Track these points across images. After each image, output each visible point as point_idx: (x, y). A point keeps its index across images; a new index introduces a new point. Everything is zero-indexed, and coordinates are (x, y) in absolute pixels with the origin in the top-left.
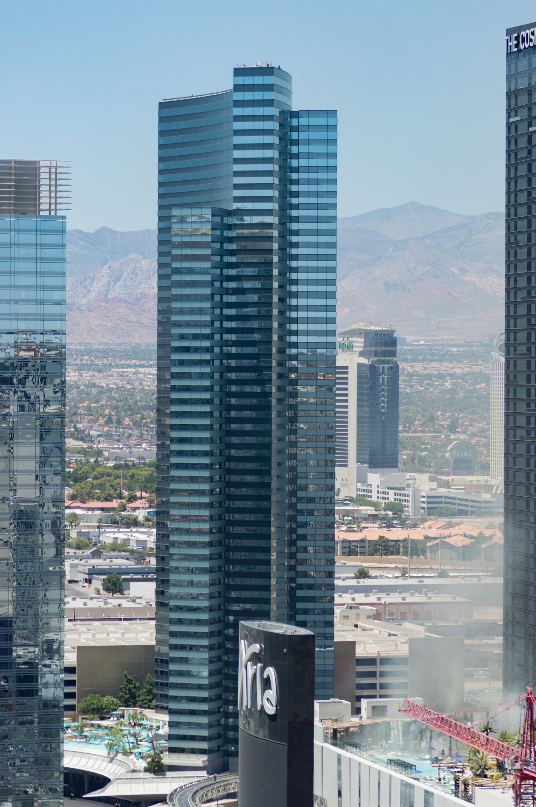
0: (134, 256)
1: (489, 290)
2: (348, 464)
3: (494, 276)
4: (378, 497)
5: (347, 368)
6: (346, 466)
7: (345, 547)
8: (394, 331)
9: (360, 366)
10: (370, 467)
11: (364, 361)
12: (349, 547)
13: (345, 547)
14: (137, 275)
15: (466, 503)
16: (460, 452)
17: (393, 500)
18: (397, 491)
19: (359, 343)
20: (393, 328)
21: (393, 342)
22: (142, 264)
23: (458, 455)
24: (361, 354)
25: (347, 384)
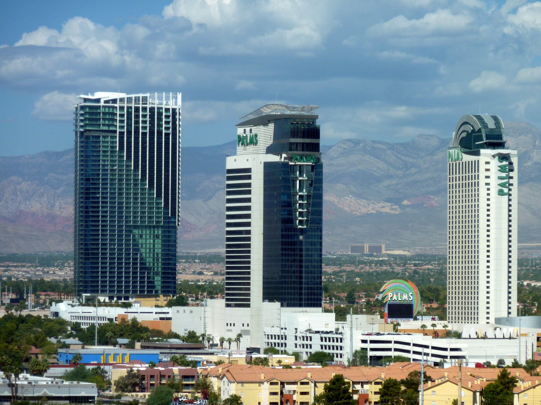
0: (14, 178)
1: (346, 209)
2: (251, 303)
3: (351, 196)
4: (296, 345)
5: (249, 170)
6: (248, 306)
7: (275, 394)
8: (316, 117)
9: (268, 166)
10: (282, 306)
11: (274, 158)
12: (282, 393)
13: (275, 394)
14: (17, 195)
15: (426, 350)
16: (397, 294)
17: (319, 349)
18: (324, 335)
19: (266, 134)
20: (315, 113)
21: (315, 133)
22: (22, 185)
23: (395, 298)
24: (270, 150)
25: (249, 192)
